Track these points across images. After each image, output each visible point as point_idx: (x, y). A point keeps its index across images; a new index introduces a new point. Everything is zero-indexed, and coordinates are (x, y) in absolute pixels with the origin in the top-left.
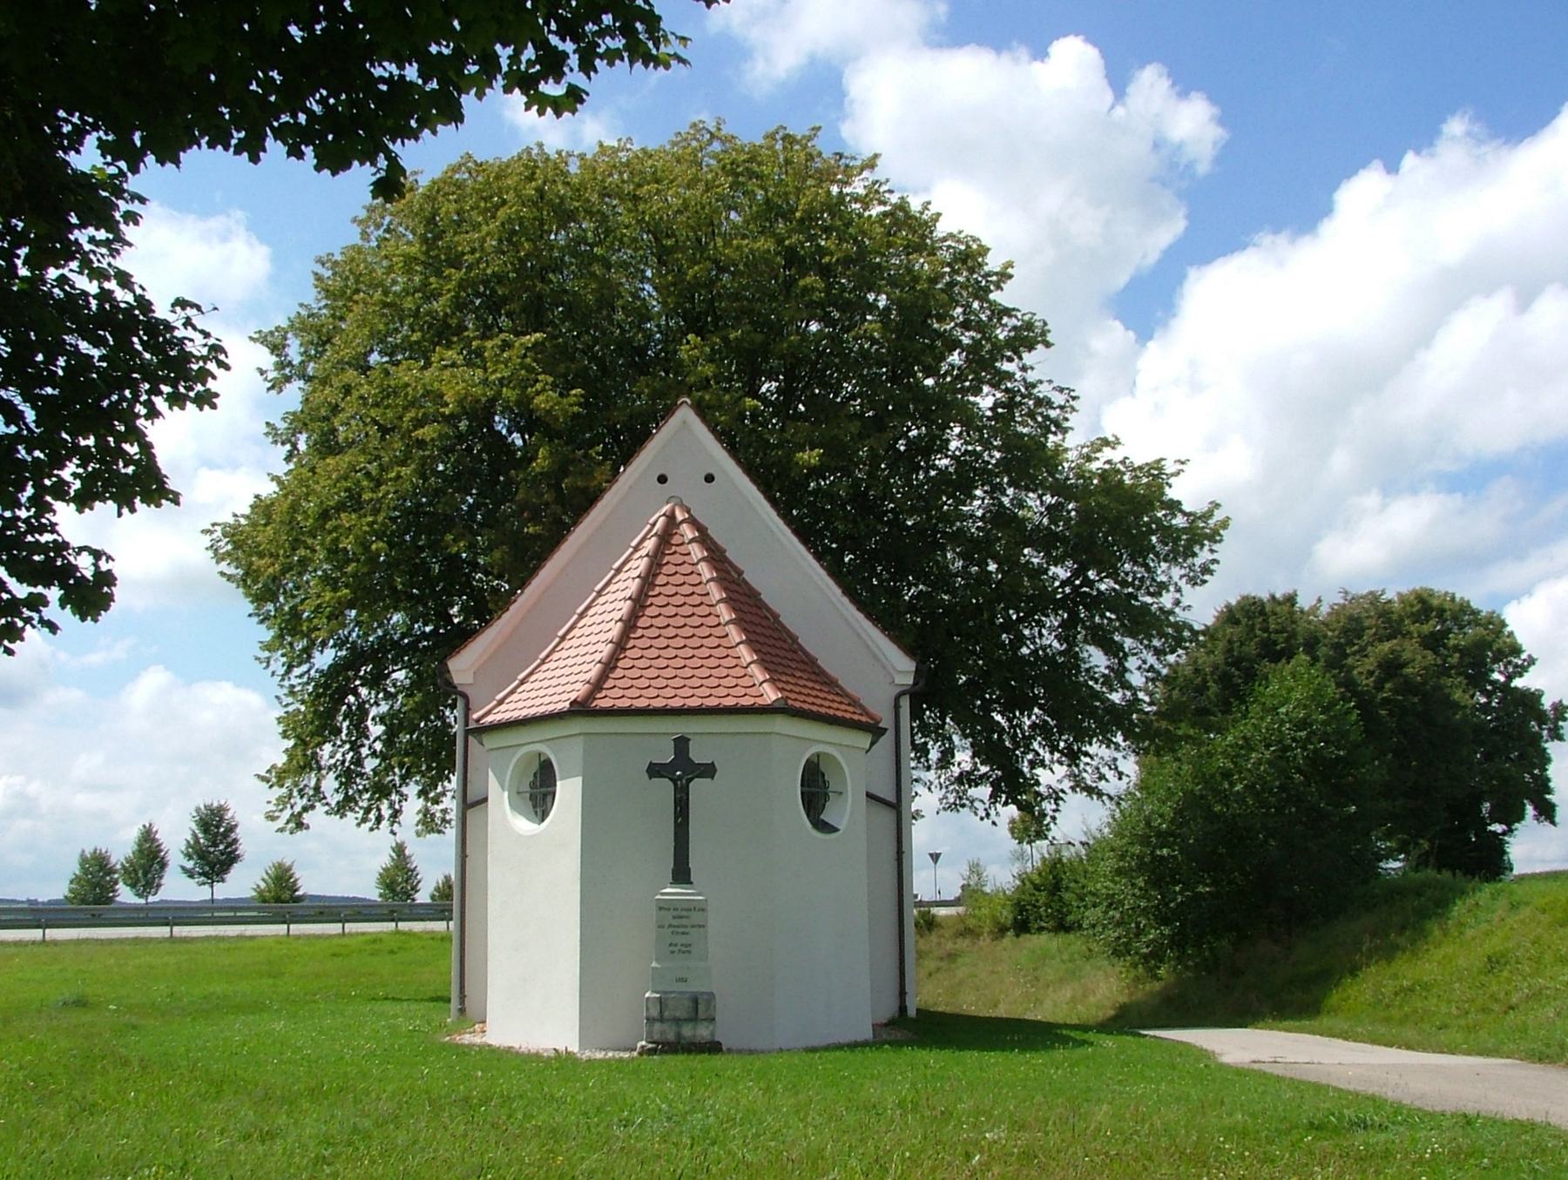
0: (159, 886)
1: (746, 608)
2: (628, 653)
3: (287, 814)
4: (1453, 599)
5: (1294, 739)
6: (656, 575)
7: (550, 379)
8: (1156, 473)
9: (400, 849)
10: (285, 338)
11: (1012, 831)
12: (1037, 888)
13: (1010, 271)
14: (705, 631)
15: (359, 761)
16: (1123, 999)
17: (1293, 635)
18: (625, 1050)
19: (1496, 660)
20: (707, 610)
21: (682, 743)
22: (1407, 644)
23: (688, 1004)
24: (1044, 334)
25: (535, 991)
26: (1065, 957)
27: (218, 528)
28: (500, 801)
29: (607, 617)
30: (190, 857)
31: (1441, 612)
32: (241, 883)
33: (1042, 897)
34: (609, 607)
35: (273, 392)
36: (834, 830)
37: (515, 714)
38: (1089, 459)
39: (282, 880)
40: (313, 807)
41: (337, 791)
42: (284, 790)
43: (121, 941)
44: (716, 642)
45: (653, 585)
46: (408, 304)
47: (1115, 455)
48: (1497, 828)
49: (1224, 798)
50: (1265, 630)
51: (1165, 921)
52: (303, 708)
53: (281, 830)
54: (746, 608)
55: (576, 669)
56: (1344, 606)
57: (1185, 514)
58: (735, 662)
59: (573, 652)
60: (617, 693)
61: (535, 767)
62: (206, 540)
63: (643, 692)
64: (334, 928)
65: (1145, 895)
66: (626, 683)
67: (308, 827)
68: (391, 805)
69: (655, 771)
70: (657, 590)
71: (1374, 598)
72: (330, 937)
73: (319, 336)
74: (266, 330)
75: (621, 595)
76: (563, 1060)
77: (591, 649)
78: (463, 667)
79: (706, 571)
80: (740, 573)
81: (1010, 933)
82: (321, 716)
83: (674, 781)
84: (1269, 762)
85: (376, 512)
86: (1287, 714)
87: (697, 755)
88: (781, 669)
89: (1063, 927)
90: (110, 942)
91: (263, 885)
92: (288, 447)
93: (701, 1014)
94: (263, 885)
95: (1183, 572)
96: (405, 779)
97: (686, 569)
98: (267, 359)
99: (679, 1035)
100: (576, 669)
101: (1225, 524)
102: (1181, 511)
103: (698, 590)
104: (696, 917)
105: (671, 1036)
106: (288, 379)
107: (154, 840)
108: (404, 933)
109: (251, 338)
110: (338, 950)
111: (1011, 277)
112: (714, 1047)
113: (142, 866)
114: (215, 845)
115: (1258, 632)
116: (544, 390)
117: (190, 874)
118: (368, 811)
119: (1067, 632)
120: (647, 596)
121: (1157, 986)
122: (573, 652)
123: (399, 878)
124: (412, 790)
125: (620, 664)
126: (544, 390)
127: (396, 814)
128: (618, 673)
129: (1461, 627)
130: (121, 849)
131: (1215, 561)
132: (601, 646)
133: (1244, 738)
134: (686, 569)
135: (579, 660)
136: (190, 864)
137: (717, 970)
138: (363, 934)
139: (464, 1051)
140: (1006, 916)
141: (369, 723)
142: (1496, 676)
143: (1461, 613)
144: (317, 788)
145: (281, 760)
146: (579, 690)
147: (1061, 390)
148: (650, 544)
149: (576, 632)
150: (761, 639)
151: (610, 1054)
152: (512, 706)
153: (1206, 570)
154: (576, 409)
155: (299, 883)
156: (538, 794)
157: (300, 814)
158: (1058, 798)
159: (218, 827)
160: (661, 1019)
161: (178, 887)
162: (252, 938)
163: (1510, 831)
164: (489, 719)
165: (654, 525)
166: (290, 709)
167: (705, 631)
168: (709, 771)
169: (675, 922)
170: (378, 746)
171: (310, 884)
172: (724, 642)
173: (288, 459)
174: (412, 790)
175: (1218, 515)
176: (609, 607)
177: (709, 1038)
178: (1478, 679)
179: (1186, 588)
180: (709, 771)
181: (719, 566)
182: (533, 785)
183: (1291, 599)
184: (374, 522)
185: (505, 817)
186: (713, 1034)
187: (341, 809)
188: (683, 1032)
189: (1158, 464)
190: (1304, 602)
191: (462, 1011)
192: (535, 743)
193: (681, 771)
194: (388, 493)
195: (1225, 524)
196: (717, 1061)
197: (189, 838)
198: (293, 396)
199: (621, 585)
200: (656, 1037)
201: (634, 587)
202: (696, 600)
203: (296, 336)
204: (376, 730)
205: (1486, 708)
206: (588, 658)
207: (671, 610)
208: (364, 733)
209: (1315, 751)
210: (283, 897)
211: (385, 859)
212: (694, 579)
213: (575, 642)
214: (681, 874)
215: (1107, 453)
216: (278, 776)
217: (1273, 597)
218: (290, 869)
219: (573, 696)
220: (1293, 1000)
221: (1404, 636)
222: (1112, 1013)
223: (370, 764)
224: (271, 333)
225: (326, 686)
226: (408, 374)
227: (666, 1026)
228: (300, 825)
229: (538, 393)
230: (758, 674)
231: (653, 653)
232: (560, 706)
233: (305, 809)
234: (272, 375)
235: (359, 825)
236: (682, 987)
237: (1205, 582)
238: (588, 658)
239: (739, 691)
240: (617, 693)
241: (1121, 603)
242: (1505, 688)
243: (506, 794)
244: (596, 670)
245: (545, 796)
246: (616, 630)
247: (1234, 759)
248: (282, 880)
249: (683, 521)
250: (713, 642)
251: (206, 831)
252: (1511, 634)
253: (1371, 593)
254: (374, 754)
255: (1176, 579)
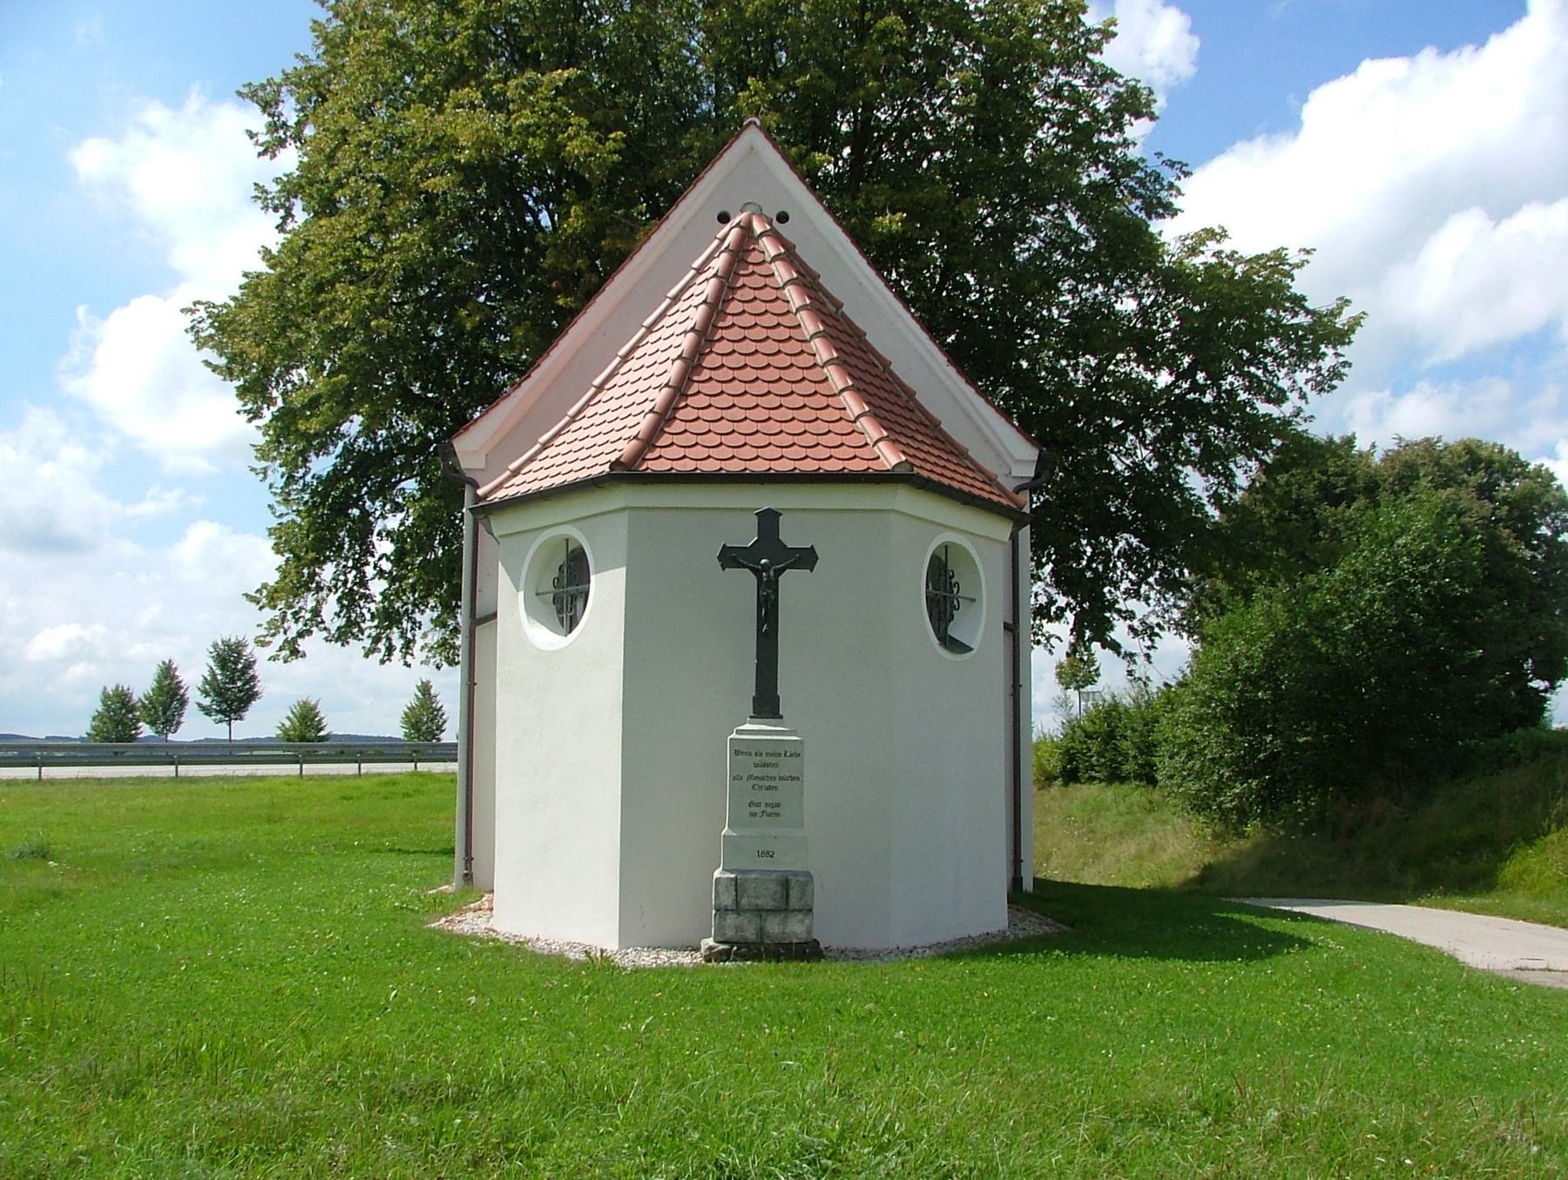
0: (179, 723)
1: (848, 349)
2: (690, 401)
3: (279, 640)
4: (1501, 451)
5: (1412, 575)
6: (727, 301)
7: (585, 123)
8: (1276, 262)
9: (425, 689)
10: (279, 92)
11: (1059, 675)
12: (1089, 736)
13: (1112, 28)
14: (796, 374)
15: (362, 582)
16: (1208, 859)
17: (1353, 479)
18: (684, 948)
19: (1543, 515)
20: (797, 347)
21: (769, 520)
22: (1463, 494)
23: (773, 887)
24: (1148, 105)
25: (561, 867)
26: (1122, 808)
27: (201, 308)
28: (511, 600)
29: (660, 357)
30: (207, 694)
31: (1490, 463)
32: (263, 721)
33: (1095, 746)
34: (662, 345)
35: (267, 157)
36: (967, 649)
37: (535, 486)
38: (1194, 251)
39: (307, 719)
40: (310, 632)
41: (338, 615)
42: (277, 612)
43: (122, 781)
44: (812, 388)
45: (698, 367)
46: (418, 46)
47: (1226, 247)
48: (1538, 684)
49: (1328, 635)
50: (1324, 473)
51: (1249, 775)
52: (299, 520)
53: (274, 658)
54: (848, 349)
55: (618, 424)
56: (1398, 453)
57: (1308, 312)
58: (837, 415)
59: (613, 404)
60: (676, 452)
61: (561, 558)
62: (187, 320)
63: (725, 414)
64: (350, 769)
65: (1230, 743)
66: (689, 439)
67: (304, 655)
68: (403, 635)
69: (730, 557)
70: (729, 321)
71: (1428, 444)
72: (347, 777)
73: (314, 88)
74: (256, 83)
75: (679, 329)
76: (598, 967)
77: (639, 398)
78: (470, 449)
79: (795, 297)
80: (839, 306)
81: (1059, 782)
82: (323, 530)
83: (756, 572)
84: (1384, 599)
85: (377, 284)
86: (1405, 546)
87: (791, 535)
88: (898, 429)
89: (1115, 777)
90: (112, 781)
91: (288, 724)
92: (282, 212)
93: (793, 903)
94: (288, 724)
95: (1310, 375)
96: (419, 604)
97: (768, 294)
98: (258, 121)
99: (761, 932)
100: (618, 424)
101: (1355, 323)
102: (1303, 307)
103: (785, 320)
104: (787, 767)
105: (750, 934)
106: (282, 143)
107: (174, 677)
108: (421, 775)
109: (239, 94)
110: (348, 792)
111: (1114, 35)
112: (808, 951)
113: (162, 704)
114: (234, 682)
115: (1317, 475)
116: (577, 135)
117: (207, 711)
118: (377, 640)
119: (1167, 447)
120: (716, 327)
121: (1245, 844)
122: (613, 404)
123: (424, 719)
124: (426, 617)
125: (680, 414)
126: (577, 135)
127: (408, 645)
128: (677, 426)
129: (1509, 480)
130: (142, 686)
131: (1345, 364)
132: (651, 394)
133: (1355, 573)
134: (768, 294)
135: (622, 413)
136: (207, 702)
137: (813, 843)
138: (380, 775)
139: (455, 948)
140: (1054, 764)
141: (374, 538)
142: (1544, 530)
143: (1511, 466)
144: (316, 612)
145: (273, 578)
146: (626, 448)
147: (1172, 164)
148: (719, 264)
149: (618, 380)
150: (872, 390)
151: (664, 956)
152: (531, 476)
153: (1336, 374)
154: (616, 157)
155: (324, 722)
156: (565, 596)
157: (294, 640)
158: (1153, 635)
159: (236, 663)
160: (737, 909)
161: (196, 726)
162: (262, 778)
163: (1553, 687)
164: (500, 494)
165: (723, 240)
166: (284, 520)
167: (796, 374)
168: (806, 559)
169: (758, 772)
170: (386, 565)
171: (335, 724)
172: (821, 388)
173: (281, 228)
174: (426, 617)
175: (1347, 314)
176: (662, 345)
177: (803, 937)
178: (1525, 532)
179: (1312, 395)
180: (806, 559)
181: (813, 294)
182: (557, 583)
183: (1349, 442)
184: (375, 296)
185: (520, 628)
186: (809, 932)
187: (342, 636)
188: (769, 930)
189: (1279, 256)
190: (1361, 445)
191: (468, 877)
192: (561, 524)
193: (768, 559)
194: (393, 261)
195: (1355, 323)
196: (819, 977)
197: (206, 674)
198: (290, 160)
199: (680, 317)
200: (730, 934)
201: (697, 316)
202: (783, 333)
203: (291, 93)
204: (386, 547)
205: (1533, 563)
206: (635, 410)
207: (748, 347)
208: (368, 550)
209: (1439, 588)
210: (306, 736)
211: (409, 698)
212: (779, 307)
213: (616, 392)
214: (766, 704)
215: (1212, 246)
216: (272, 596)
217: (1331, 441)
218: (315, 707)
219: (613, 457)
220: (1462, 873)
221: (1460, 485)
222: (1193, 873)
223: (377, 587)
224: (263, 87)
225: (325, 495)
226: (415, 119)
227: (743, 920)
228: (295, 652)
229: (570, 138)
230: (871, 429)
231: (725, 401)
232: (595, 471)
233: (301, 635)
234: (263, 138)
235: (367, 656)
236: (765, 864)
237: (1334, 387)
238: (635, 410)
239: (845, 452)
240: (676, 452)
241: (1228, 411)
242: (1551, 542)
243: (521, 594)
244: (645, 422)
245: (574, 598)
246: (673, 370)
247: (1342, 596)
248: (307, 719)
249: (762, 235)
250: (807, 388)
251: (223, 667)
252: (1560, 488)
253: (1427, 440)
254: (381, 573)
255: (1301, 383)
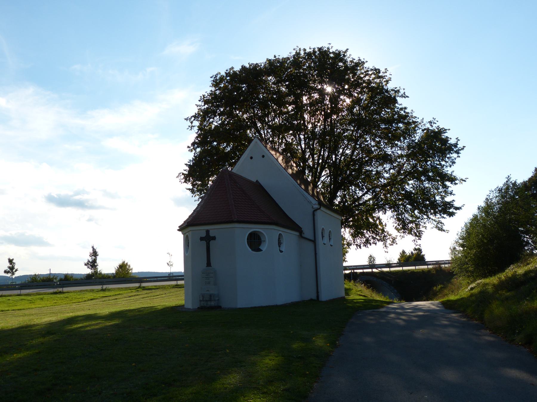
21: (208, 232)
160: (203, 301)
180: (214, 238)
